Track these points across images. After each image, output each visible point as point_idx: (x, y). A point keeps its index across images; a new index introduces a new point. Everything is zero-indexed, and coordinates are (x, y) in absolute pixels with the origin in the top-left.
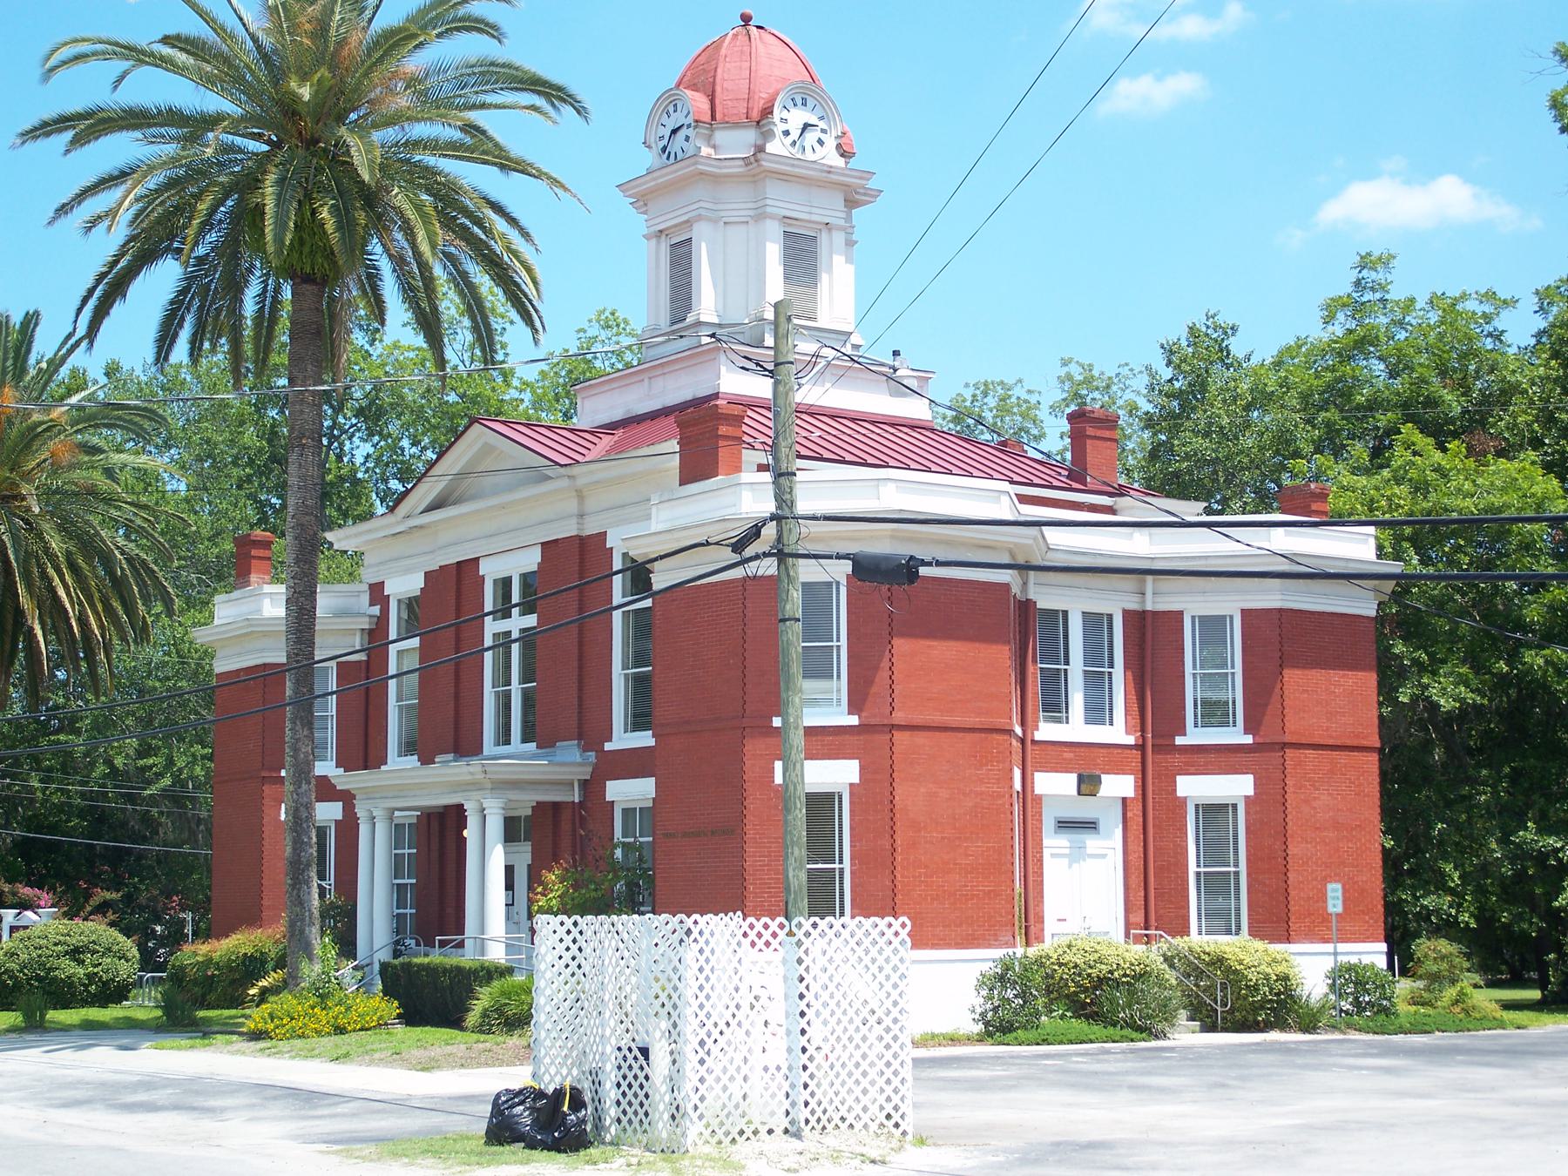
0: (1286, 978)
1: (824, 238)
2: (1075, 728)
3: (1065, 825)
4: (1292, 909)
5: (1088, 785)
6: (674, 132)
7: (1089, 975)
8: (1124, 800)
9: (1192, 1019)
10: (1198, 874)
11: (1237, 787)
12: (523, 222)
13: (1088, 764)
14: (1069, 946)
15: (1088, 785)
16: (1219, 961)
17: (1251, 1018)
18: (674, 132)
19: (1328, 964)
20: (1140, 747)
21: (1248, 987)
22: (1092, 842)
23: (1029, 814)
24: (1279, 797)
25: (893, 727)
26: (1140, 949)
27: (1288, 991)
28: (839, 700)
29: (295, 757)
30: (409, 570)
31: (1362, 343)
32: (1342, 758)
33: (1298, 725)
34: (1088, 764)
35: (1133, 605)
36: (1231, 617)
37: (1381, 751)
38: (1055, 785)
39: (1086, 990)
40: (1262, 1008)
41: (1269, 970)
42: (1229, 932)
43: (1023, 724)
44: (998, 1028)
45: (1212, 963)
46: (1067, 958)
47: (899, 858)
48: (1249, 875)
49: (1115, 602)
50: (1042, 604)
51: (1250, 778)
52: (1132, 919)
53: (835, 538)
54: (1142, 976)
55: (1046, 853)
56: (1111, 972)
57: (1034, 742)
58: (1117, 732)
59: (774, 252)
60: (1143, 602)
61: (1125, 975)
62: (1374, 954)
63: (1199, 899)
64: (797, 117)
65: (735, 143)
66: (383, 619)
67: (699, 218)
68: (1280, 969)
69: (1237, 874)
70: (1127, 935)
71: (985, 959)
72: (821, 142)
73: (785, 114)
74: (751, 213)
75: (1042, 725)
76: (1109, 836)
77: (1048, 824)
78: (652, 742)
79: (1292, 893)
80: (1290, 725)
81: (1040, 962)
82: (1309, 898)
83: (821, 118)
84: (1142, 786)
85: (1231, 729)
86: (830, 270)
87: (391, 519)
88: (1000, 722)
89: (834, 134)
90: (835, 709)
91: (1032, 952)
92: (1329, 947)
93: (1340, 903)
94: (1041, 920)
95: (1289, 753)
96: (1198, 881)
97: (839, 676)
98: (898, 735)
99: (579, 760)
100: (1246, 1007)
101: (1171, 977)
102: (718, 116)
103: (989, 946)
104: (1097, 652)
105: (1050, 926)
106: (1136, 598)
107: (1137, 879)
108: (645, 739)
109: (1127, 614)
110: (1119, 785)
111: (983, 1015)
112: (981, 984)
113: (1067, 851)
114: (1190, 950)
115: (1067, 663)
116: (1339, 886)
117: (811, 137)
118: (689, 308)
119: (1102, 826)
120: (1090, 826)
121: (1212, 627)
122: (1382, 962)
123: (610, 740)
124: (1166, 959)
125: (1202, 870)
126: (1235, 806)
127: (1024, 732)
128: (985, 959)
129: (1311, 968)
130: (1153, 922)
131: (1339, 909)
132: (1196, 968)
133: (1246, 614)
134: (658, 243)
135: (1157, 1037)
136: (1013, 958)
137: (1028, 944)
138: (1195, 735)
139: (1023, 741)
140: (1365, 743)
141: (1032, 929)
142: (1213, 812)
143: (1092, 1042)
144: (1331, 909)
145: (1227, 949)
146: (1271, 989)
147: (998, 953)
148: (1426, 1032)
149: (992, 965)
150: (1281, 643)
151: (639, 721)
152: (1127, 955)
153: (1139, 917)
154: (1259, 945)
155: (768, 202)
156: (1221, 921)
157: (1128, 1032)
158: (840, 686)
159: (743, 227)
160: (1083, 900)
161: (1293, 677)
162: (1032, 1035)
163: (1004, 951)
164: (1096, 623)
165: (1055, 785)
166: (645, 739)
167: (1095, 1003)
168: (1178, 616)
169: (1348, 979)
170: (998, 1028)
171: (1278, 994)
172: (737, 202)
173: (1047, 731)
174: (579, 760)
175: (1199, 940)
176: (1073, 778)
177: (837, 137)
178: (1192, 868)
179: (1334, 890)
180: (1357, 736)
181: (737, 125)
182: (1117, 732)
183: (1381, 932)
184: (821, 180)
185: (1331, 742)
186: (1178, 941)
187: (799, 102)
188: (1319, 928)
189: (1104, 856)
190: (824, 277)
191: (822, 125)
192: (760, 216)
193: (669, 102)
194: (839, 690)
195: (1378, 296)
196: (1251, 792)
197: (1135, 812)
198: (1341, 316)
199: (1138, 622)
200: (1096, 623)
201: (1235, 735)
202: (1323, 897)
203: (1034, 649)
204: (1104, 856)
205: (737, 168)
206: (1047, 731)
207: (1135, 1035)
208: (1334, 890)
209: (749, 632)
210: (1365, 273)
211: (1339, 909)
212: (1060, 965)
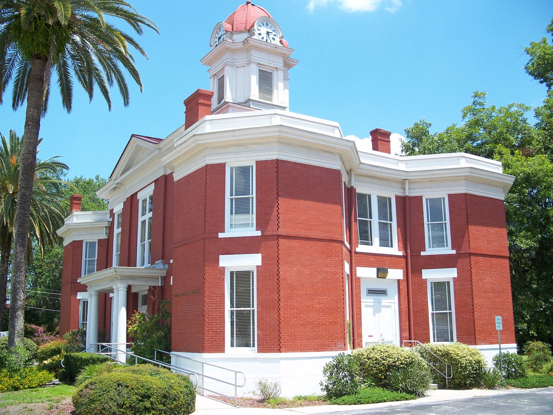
0: (479, 362)
1: (275, 74)
2: (375, 248)
3: (371, 292)
4: (477, 329)
5: (382, 273)
6: (219, 38)
7: (383, 364)
8: (399, 280)
9: (434, 383)
10: (433, 314)
11: (449, 274)
12: (141, 46)
13: (382, 264)
14: (373, 349)
15: (382, 273)
16: (447, 354)
17: (463, 382)
18: (219, 38)
20: (405, 257)
21: (461, 367)
22: (384, 301)
23: (354, 286)
24: (469, 278)
25: (279, 237)
26: (407, 349)
27: (480, 368)
28: (252, 224)
29: (16, 260)
30: (119, 203)
31: (477, 123)
32: (495, 261)
34: (382, 264)
35: (400, 194)
36: (444, 198)
37: (510, 259)
38: (366, 273)
39: (381, 371)
40: (468, 377)
41: (471, 358)
42: (447, 340)
43: (350, 243)
44: (335, 394)
45: (442, 356)
46: (372, 355)
47: (282, 304)
48: (456, 314)
49: (392, 194)
50: (359, 191)
51: (455, 270)
52: (403, 335)
53: (251, 144)
54: (411, 364)
55: (363, 305)
56: (394, 362)
57: (356, 253)
58: (395, 250)
59: (254, 79)
60: (404, 193)
61: (402, 364)
62: (511, 348)
63: (433, 325)
64: (264, 30)
65: (240, 38)
66: (112, 223)
67: (226, 65)
68: (476, 358)
69: (450, 313)
70: (401, 343)
71: (328, 357)
72: (273, 39)
73: (259, 28)
74: (246, 62)
75: (359, 246)
76: (393, 299)
77: (364, 292)
79: (476, 321)
80: (472, 246)
81: (358, 358)
82: (484, 324)
83: (274, 31)
84: (406, 275)
85: (445, 248)
86: (277, 89)
87: (112, 182)
88: (337, 237)
89: (279, 36)
90: (250, 229)
91: (356, 351)
92: (497, 346)
93: (501, 325)
94: (360, 336)
95: (473, 258)
97: (252, 213)
98: (281, 241)
99: (162, 267)
100: (459, 376)
101: (424, 363)
102: (234, 30)
103: (332, 350)
104: (384, 212)
105: (365, 339)
107: (405, 317)
109: (397, 197)
110: (396, 274)
111: (327, 387)
112: (325, 371)
113: (372, 304)
114: (432, 349)
115: (371, 218)
116: (500, 317)
117: (271, 36)
118: (223, 98)
119: (389, 292)
120: (383, 292)
121: (435, 204)
122: (515, 351)
124: (422, 353)
125: (434, 312)
126: (448, 283)
127: (351, 247)
128: (328, 357)
129: (487, 355)
130: (413, 336)
131: (501, 328)
132: (434, 358)
133: (451, 197)
134: (214, 79)
135: (419, 396)
136: (342, 356)
137: (354, 348)
138: (430, 251)
139: (350, 252)
140: (504, 254)
141: (356, 341)
142: (440, 286)
143: (385, 401)
144: (497, 328)
145: (450, 349)
146: (473, 368)
147: (336, 353)
148: (545, 387)
149: (331, 360)
150: (468, 209)
152: (402, 353)
153: (406, 334)
154: (463, 346)
155: (252, 57)
156: (442, 336)
157: (404, 394)
158: (252, 218)
159: (243, 68)
160: (380, 327)
162: (351, 398)
163: (339, 352)
164: (384, 202)
165: (366, 273)
167: (388, 377)
168: (421, 197)
169: (502, 361)
170: (335, 394)
171: (476, 370)
172: (241, 58)
173: (361, 248)
174: (162, 267)
175: (434, 344)
176: (375, 270)
177: (280, 38)
178: (430, 311)
179: (498, 319)
180: (500, 251)
181: (241, 32)
182: (395, 250)
183: (514, 338)
184: (273, 51)
185: (490, 253)
186: (425, 345)
187: (265, 24)
188: (490, 337)
189: (390, 306)
190: (275, 91)
191: (274, 33)
192: (249, 63)
193: (219, 27)
194: (252, 219)
195: (481, 107)
196: (455, 275)
197: (404, 286)
198: (468, 115)
199: (403, 201)
200: (384, 202)
201: (448, 250)
202: (494, 324)
203: (355, 210)
204: (390, 306)
205: (240, 46)
206: (361, 248)
207: (408, 396)
208: (498, 319)
209: (208, 192)
210: (476, 99)
211: (501, 328)
212: (369, 359)
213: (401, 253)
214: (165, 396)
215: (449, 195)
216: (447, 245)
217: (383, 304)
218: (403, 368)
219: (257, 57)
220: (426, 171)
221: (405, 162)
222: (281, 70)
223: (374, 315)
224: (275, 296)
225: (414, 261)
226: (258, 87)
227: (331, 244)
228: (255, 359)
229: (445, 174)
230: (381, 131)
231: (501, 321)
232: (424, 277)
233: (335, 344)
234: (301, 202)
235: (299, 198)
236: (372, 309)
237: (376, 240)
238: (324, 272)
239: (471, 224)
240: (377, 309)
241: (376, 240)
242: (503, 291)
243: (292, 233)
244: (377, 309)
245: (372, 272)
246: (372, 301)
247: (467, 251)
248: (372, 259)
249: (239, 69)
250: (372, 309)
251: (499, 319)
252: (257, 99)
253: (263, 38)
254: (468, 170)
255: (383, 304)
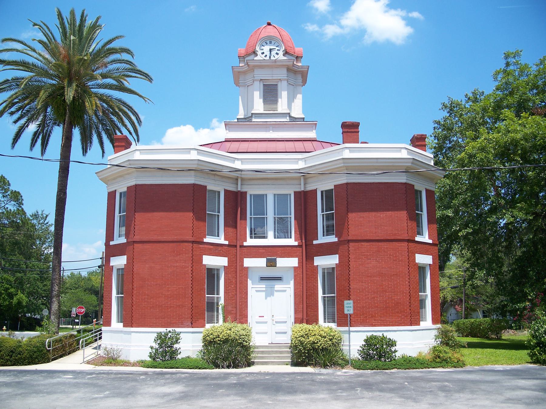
2: (271, 240)
19: (364, 336)
22: (278, 286)
33: (353, 232)
34: (271, 254)
36: (290, 194)
72: (277, 54)
78: (336, 240)
96: (324, 301)
106: (235, 186)
108: (333, 239)
113: (264, 289)
117: (273, 53)
123: (246, 241)
131: (351, 312)
151: (328, 231)
161: (352, 216)
166: (333, 239)
185: (377, 238)
187: (268, 42)
189: (285, 291)
190: (280, 100)
191: (277, 48)
204: (285, 291)
213: (296, 244)
214: (12, 351)
215: (295, 192)
216: (291, 235)
217: (276, 289)
218: (219, 344)
219: (260, 74)
220: (311, 167)
221: (304, 160)
222: (284, 80)
223: (266, 298)
224: (131, 286)
225: (308, 250)
226: (262, 100)
227: (182, 244)
228: (121, 332)
229: (326, 167)
230: (347, 124)
231: (352, 305)
232: (315, 264)
233: (182, 322)
234: (156, 214)
235: (153, 211)
236: (264, 293)
237: (271, 234)
238: (174, 266)
239: (352, 212)
240: (269, 293)
241: (271, 234)
242: (396, 275)
243: (145, 238)
244: (269, 293)
245: (261, 262)
246: (264, 286)
247: (346, 238)
248: (261, 250)
249: (249, 87)
250: (264, 293)
251: (350, 304)
252: (262, 111)
253: (266, 56)
254: (196, 162)
255: (276, 289)
